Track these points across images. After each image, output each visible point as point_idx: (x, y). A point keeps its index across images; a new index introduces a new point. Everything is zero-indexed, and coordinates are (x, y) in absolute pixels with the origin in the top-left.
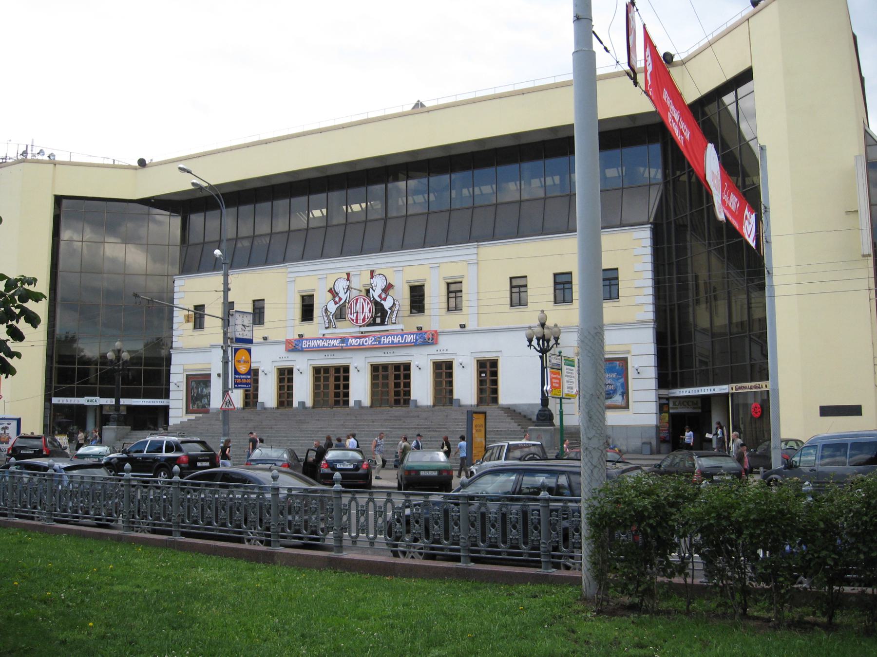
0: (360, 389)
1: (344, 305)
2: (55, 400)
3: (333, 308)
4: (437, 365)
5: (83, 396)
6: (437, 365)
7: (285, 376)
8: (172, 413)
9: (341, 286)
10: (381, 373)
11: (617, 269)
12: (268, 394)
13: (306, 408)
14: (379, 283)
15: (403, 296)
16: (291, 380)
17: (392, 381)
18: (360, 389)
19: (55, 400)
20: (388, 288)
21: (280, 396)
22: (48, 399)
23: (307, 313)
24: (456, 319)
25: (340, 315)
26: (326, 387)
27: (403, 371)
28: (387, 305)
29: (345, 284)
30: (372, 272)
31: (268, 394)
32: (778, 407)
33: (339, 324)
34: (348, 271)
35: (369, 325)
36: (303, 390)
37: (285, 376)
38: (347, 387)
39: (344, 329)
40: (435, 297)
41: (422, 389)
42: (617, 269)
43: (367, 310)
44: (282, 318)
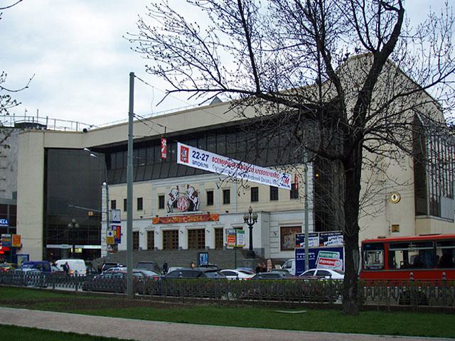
0: (183, 242)
1: (176, 201)
2: (48, 246)
3: (171, 203)
4: (217, 230)
5: (60, 244)
6: (217, 230)
7: (151, 235)
8: (102, 252)
9: (174, 193)
10: (192, 233)
11: (46, 149)
12: (143, 244)
13: (159, 250)
14: (191, 191)
15: (203, 197)
16: (138, 237)
17: (197, 237)
18: (183, 242)
19: (48, 246)
20: (195, 194)
21: (148, 244)
22: (44, 245)
23: (161, 206)
24: (227, 207)
25: (175, 205)
26: (194, 239)
27: (175, 233)
28: (195, 201)
29: (176, 191)
30: (188, 186)
31: (143, 244)
32: (128, 245)
33: (174, 210)
34: (177, 184)
35: (189, 211)
36: (159, 243)
37: (151, 235)
38: (204, 239)
39: (176, 213)
40: (218, 197)
41: (210, 242)
42: (46, 149)
43: (186, 205)
44: (151, 205)
